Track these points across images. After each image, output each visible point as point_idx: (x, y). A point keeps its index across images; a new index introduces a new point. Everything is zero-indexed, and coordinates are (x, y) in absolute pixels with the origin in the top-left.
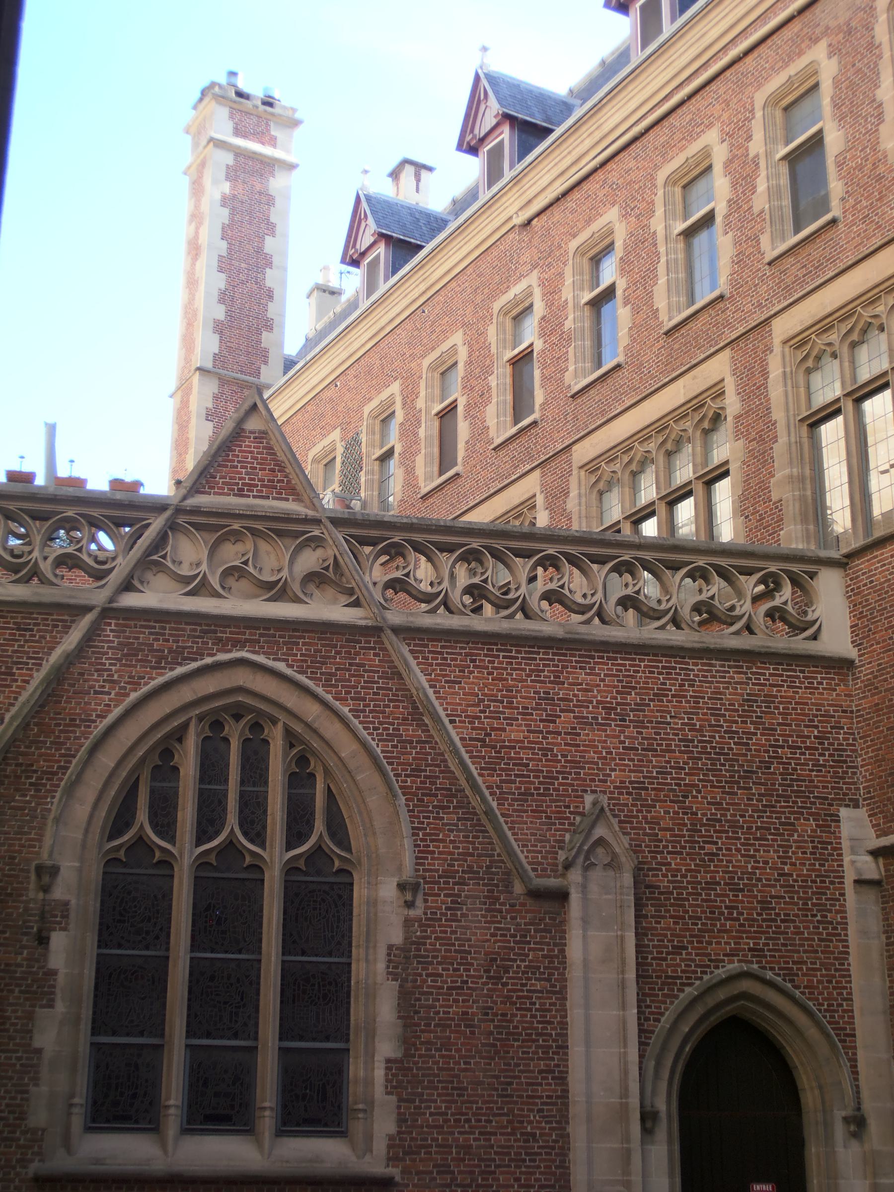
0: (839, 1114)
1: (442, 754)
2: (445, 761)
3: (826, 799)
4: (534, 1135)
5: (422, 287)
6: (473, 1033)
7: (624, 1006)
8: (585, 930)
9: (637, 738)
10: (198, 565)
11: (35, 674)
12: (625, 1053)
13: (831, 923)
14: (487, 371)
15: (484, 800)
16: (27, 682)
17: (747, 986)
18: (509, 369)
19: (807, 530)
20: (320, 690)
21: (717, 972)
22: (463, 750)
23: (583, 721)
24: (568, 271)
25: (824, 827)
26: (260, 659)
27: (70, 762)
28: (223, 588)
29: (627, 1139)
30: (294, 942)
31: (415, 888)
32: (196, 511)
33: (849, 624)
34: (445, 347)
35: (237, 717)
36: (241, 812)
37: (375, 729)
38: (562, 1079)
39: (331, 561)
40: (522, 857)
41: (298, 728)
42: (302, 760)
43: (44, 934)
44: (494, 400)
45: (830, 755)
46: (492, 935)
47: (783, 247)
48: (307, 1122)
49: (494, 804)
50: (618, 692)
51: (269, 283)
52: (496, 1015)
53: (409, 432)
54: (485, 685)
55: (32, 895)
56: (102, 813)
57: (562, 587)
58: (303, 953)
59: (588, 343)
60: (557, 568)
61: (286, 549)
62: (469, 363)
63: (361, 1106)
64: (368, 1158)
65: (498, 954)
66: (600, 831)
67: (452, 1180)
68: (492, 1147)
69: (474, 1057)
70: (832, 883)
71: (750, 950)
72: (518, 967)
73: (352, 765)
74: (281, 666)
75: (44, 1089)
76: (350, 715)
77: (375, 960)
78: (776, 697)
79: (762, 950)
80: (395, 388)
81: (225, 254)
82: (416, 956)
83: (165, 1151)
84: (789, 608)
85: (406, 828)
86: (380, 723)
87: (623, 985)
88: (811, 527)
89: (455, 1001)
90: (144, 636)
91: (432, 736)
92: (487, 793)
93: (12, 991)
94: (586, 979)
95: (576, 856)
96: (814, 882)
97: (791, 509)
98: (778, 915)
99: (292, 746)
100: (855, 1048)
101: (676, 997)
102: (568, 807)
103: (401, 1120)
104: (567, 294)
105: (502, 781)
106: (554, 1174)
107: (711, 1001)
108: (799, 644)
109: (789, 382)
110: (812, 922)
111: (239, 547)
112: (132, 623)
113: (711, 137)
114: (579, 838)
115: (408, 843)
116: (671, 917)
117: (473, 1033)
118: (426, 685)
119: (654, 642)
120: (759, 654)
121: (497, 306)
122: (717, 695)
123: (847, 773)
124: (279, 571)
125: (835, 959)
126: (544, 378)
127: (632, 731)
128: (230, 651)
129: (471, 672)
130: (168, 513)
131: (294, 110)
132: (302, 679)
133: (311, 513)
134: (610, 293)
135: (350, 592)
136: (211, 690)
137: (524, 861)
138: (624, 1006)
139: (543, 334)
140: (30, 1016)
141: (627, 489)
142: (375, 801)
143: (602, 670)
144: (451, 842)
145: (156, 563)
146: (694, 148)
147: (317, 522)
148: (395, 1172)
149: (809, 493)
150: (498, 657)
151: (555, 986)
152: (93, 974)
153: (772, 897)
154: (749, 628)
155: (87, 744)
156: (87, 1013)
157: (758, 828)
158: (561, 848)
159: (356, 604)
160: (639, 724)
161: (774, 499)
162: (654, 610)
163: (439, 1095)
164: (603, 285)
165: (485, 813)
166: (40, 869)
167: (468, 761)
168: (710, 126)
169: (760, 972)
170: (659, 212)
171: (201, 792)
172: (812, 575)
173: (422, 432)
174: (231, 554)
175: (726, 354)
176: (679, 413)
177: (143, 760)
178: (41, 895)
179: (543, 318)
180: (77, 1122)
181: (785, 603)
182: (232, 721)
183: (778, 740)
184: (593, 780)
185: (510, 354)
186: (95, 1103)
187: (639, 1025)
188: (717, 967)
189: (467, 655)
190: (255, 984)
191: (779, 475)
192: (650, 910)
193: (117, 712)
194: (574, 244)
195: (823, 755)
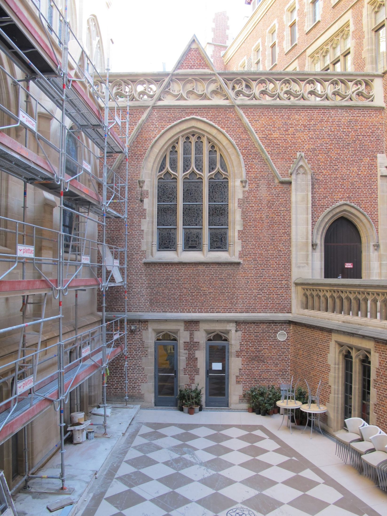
0: (372, 244)
1: (253, 143)
2: (254, 144)
3: (373, 151)
4: (281, 250)
6: (263, 223)
7: (307, 214)
8: (296, 192)
9: (313, 135)
10: (180, 91)
11: (135, 127)
12: (308, 227)
13: (373, 189)
14: (283, 30)
15: (266, 155)
16: (133, 129)
17: (345, 208)
18: (289, 29)
19: (373, 67)
20: (216, 126)
21: (336, 204)
22: (260, 141)
23: (297, 130)
27: (146, 151)
28: (187, 97)
29: (307, 251)
30: (212, 199)
31: (246, 182)
32: (178, 75)
33: (383, 96)
34: (272, 25)
35: (193, 135)
36: (195, 162)
37: (233, 136)
38: (289, 235)
39: (219, 86)
40: (278, 172)
41: (211, 137)
42: (213, 147)
43: (142, 199)
44: (285, 39)
45: (375, 138)
46: (269, 195)
49: (269, 157)
50: (308, 121)
52: (270, 217)
54: (266, 121)
55: (138, 189)
56: (156, 165)
57: (291, 89)
58: (215, 202)
59: (311, 16)
60: (289, 83)
61: (205, 84)
62: (279, 29)
63: (231, 243)
64: (233, 257)
65: (270, 200)
66: (301, 163)
67: (257, 263)
68: (269, 254)
69: (263, 229)
70: (374, 177)
71: (347, 197)
72: (277, 204)
73: (226, 147)
74: (205, 119)
76: (226, 133)
77: (235, 203)
78: (358, 120)
79: (351, 197)
82: (246, 202)
83: (178, 256)
84: (364, 92)
85: (243, 165)
86: (235, 134)
87: (307, 208)
88: (374, 66)
89: (258, 214)
90: (165, 113)
91: (250, 137)
92: (267, 153)
93: (135, 215)
94: (296, 207)
95: (294, 171)
96: (368, 176)
97: (368, 60)
98: (356, 187)
99: (209, 143)
100: (378, 225)
101: (324, 211)
102: (292, 156)
103: (243, 247)
105: (272, 150)
106: (287, 261)
107: (334, 212)
108: (366, 103)
109: (369, 17)
110: (367, 188)
111: (192, 85)
112: (161, 110)
114: (295, 165)
115: (244, 169)
116: (323, 188)
117: (263, 223)
118: (248, 122)
119: (319, 105)
120: (353, 107)
121: (286, 9)
122: (339, 120)
123: (380, 143)
124: (204, 91)
125: (374, 199)
126: (299, 30)
128: (190, 116)
129: (262, 117)
130: (170, 76)
132: (211, 123)
133: (212, 72)
135: (225, 95)
137: (278, 173)
138: (307, 214)
139: (298, 15)
140: (140, 221)
141: (322, 62)
142: (233, 157)
144: (257, 168)
145: (167, 92)
147: (214, 75)
148: (241, 261)
149: (374, 54)
150: (270, 112)
151: (287, 209)
152: (157, 210)
153: (355, 181)
155: (150, 146)
156: (156, 220)
157: (351, 161)
158: (290, 169)
159: (227, 99)
160: (314, 130)
161: (363, 57)
162: (320, 95)
163: (253, 240)
165: (266, 159)
166: (139, 182)
167: (261, 144)
171: (184, 158)
172: (372, 81)
173: (267, 53)
174: (189, 87)
175: (350, 11)
177: (166, 150)
178: (140, 189)
180: (155, 248)
181: (363, 90)
182: (192, 137)
183: (358, 134)
184: (300, 148)
187: (312, 219)
188: (337, 202)
189: (261, 112)
190: (201, 210)
191: (364, 50)
192: (316, 186)
193: (158, 136)
195: (373, 138)
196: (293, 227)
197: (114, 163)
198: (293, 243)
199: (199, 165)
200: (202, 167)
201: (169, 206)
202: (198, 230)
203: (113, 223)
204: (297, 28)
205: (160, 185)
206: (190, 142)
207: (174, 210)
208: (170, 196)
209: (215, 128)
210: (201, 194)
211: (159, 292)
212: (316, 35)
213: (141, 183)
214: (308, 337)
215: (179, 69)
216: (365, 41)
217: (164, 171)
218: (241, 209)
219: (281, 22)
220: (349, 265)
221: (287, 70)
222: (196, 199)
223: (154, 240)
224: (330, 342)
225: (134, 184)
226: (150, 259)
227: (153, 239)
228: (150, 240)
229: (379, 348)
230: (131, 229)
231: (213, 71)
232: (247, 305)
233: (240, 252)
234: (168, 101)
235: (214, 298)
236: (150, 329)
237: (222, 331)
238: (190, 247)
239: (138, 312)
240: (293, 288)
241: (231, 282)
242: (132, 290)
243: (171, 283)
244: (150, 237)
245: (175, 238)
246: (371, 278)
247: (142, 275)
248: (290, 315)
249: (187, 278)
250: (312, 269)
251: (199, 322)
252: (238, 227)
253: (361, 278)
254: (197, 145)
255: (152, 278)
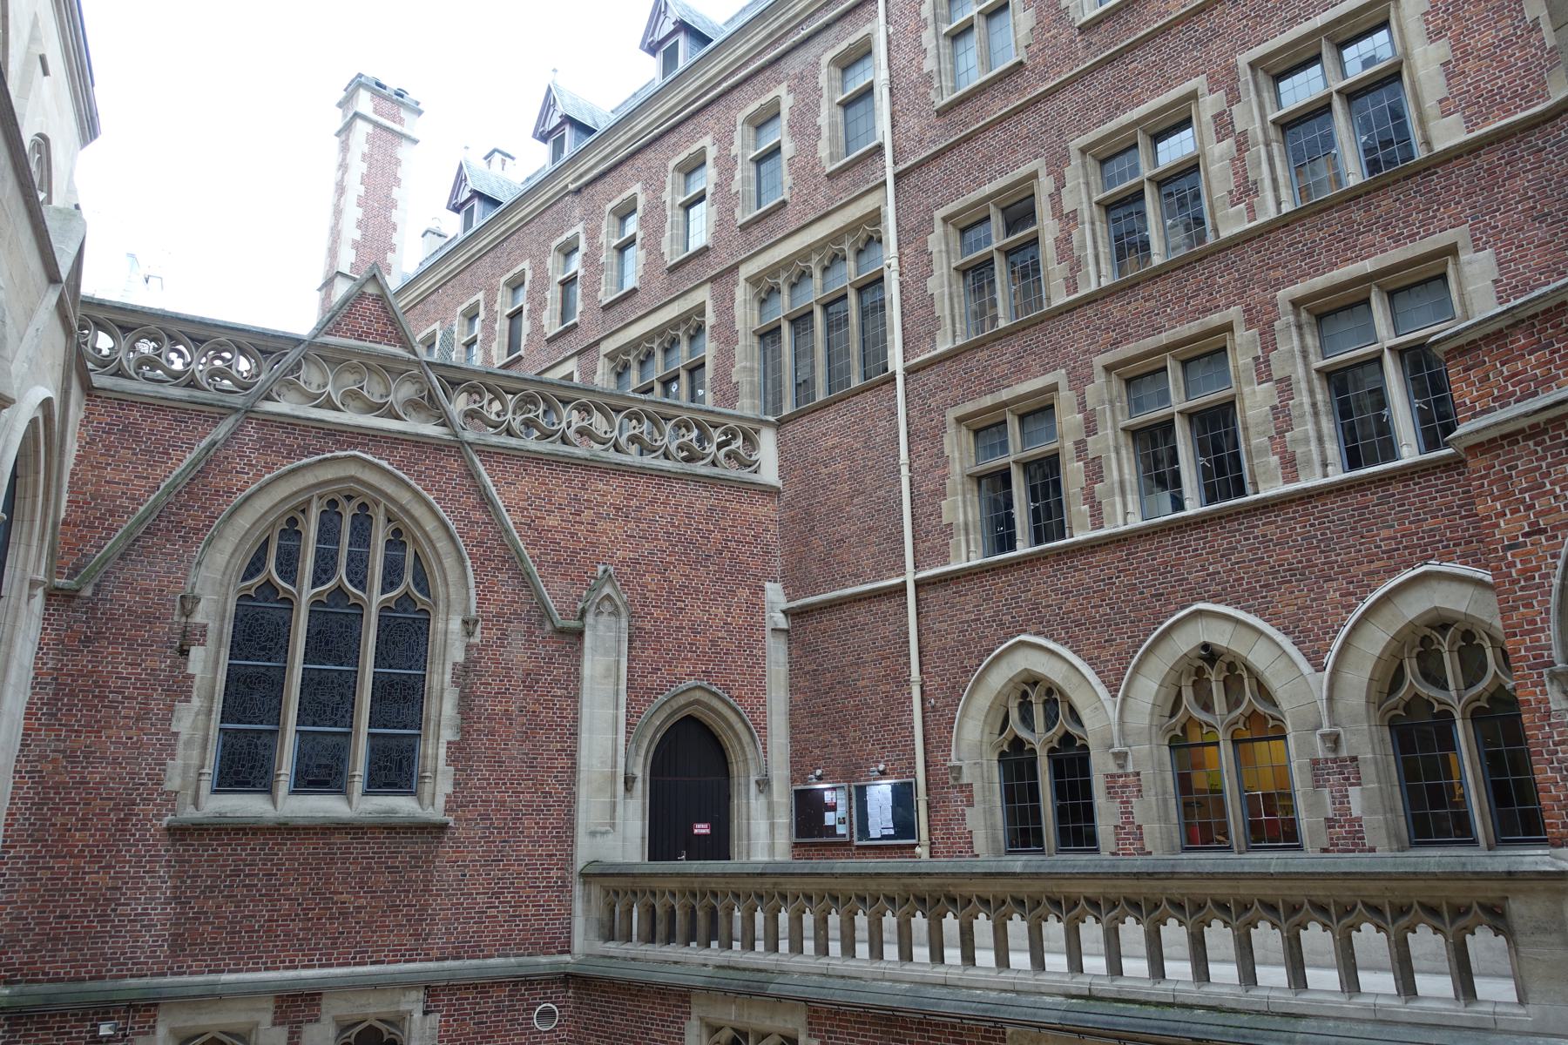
0: (753, 779)
5: (503, 229)
7: (617, 707)
14: (545, 288)
16: (181, 461)
17: (698, 695)
20: (412, 482)
24: (604, 224)
25: (755, 594)
26: (369, 457)
35: (349, 498)
36: (348, 565)
47: (749, 217)
48: (238, 783)
49: (535, 569)
51: (394, 219)
53: (489, 326)
58: (390, 667)
59: (615, 273)
66: (607, 590)
74: (384, 464)
75: (179, 762)
80: (480, 296)
81: (363, 194)
89: (500, 702)
103: (456, 784)
104: (603, 239)
107: (675, 704)
108: (745, 474)
113: (707, 141)
115: (473, 592)
118: (491, 484)
121: (554, 244)
122: (690, 505)
126: (584, 295)
127: (632, 525)
131: (418, 103)
134: (631, 241)
136: (330, 477)
138: (617, 707)
139: (585, 264)
140: (171, 709)
143: (615, 483)
145: (291, 383)
146: (695, 147)
148: (451, 820)
154: (714, 464)
156: (218, 707)
159: (444, 425)
160: (638, 520)
164: (627, 235)
168: (706, 134)
169: (709, 687)
170: (669, 188)
172: (757, 432)
173: (497, 327)
176: (674, 324)
177: (273, 525)
178: (184, 620)
179: (585, 254)
180: (206, 786)
182: (345, 502)
185: (560, 277)
186: (220, 772)
191: (737, 366)
192: (637, 644)
193: (254, 487)
194: (610, 206)
196: (584, 737)
197: (110, 543)
198: (583, 775)
199: (356, 573)
200: (366, 577)
201: (263, 670)
202: (338, 739)
203: (81, 711)
204: (578, 290)
205: (241, 614)
206: (340, 514)
207: (276, 684)
208: (268, 644)
209: (409, 486)
210: (355, 646)
211: (206, 913)
212: (627, 315)
213: (188, 603)
214: (621, 1014)
215: (327, 333)
216: (738, 349)
217: (258, 580)
218: (458, 690)
219: (539, 267)
220: (702, 829)
221: (549, 376)
222: (340, 657)
223: (207, 762)
224: (686, 1022)
225: (164, 605)
226: (188, 813)
227: (203, 759)
228: (195, 761)
229: (819, 1024)
230: (139, 729)
231: (416, 355)
232: (457, 938)
233: (448, 796)
234: (284, 406)
235: (368, 924)
236: (162, 1031)
237: (381, 1017)
238: (310, 783)
239: (125, 976)
240: (578, 890)
241: (418, 876)
242: (114, 910)
243: (244, 886)
244: (196, 753)
245: (271, 759)
246: (753, 859)
247: (157, 862)
248: (567, 958)
249: (297, 870)
250: (624, 839)
251: (156, 1005)
252: (448, 734)
253: (729, 858)
254: (357, 523)
255: (185, 872)
